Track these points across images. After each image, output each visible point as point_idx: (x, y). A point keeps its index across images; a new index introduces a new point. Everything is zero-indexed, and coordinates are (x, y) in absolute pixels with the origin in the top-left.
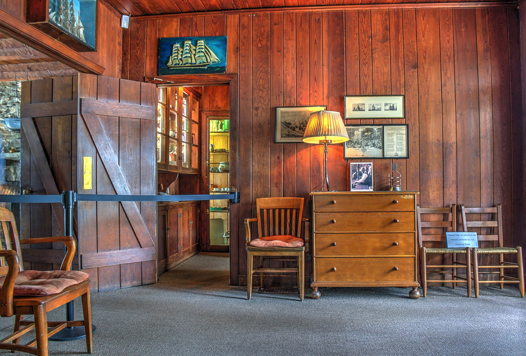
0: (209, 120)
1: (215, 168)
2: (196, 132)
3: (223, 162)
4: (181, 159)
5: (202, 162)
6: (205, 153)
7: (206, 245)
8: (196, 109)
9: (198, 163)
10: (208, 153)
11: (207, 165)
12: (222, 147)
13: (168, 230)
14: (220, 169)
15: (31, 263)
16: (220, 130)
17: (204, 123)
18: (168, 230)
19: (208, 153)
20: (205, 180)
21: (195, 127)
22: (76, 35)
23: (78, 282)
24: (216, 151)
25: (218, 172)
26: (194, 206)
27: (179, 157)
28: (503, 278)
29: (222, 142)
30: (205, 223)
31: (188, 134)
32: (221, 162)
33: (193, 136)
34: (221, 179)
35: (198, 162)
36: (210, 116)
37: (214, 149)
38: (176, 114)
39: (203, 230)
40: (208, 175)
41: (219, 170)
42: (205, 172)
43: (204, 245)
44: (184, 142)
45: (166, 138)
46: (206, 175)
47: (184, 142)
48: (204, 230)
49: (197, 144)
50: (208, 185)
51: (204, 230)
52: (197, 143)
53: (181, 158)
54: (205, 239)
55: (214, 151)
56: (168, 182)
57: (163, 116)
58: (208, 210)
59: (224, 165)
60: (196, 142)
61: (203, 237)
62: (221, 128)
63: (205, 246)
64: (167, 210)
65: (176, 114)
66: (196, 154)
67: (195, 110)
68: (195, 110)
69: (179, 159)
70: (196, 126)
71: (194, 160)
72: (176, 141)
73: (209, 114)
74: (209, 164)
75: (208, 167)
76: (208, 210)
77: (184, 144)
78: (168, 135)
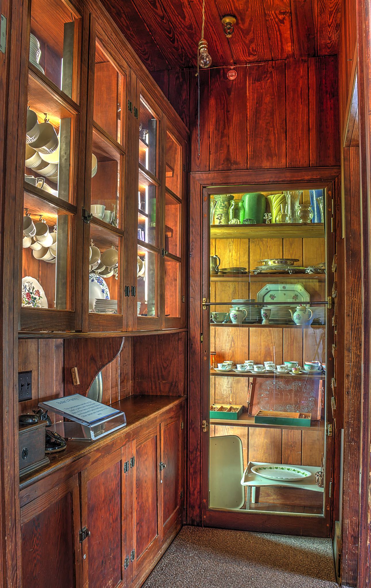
0: (209, 195)
1: (219, 314)
2: (176, 225)
3: (241, 301)
4: (133, 295)
5: (191, 300)
6: (198, 277)
7: (199, 507)
8: (175, 168)
9: (182, 302)
10: (205, 276)
11: (204, 308)
12: (235, 264)
13: (81, 539)
14: (236, 317)
15: (249, 239)
16: (233, 222)
17: (195, 204)
18: (81, 539)
19: (205, 276)
20: (197, 346)
21: (173, 211)
22: (44, 147)
23: (154, 311)
24: (224, 273)
25: (229, 324)
26: (171, 418)
27: (127, 288)
28: (263, 324)
29: (236, 252)
30: (198, 453)
31: (154, 232)
32: (234, 301)
33: (169, 234)
34: (233, 340)
35: (182, 299)
36: (212, 184)
37: (220, 268)
38: (117, 156)
39: (192, 471)
40: (205, 333)
41: (232, 319)
42: (198, 326)
43: (193, 507)
44: (143, 244)
45: (73, 219)
46: (201, 334)
47: (143, 244)
48: (195, 472)
49: (178, 255)
50: (205, 358)
51: (195, 472)
52: (178, 193)
53: (133, 289)
54: (196, 492)
55: (219, 274)
56: (95, 361)
57: (68, 144)
58: (205, 422)
59: (242, 308)
60: (176, 249)
61: (192, 490)
62: (236, 215)
63: (197, 511)
64: (80, 474)
65: (117, 156)
66: (176, 280)
67: (173, 170)
68: (173, 170)
69: (127, 295)
70: (176, 209)
71: (171, 296)
72: (116, 239)
73: (207, 179)
74: (208, 306)
75: (205, 314)
76: (205, 422)
77: (143, 251)
78: (84, 211)
